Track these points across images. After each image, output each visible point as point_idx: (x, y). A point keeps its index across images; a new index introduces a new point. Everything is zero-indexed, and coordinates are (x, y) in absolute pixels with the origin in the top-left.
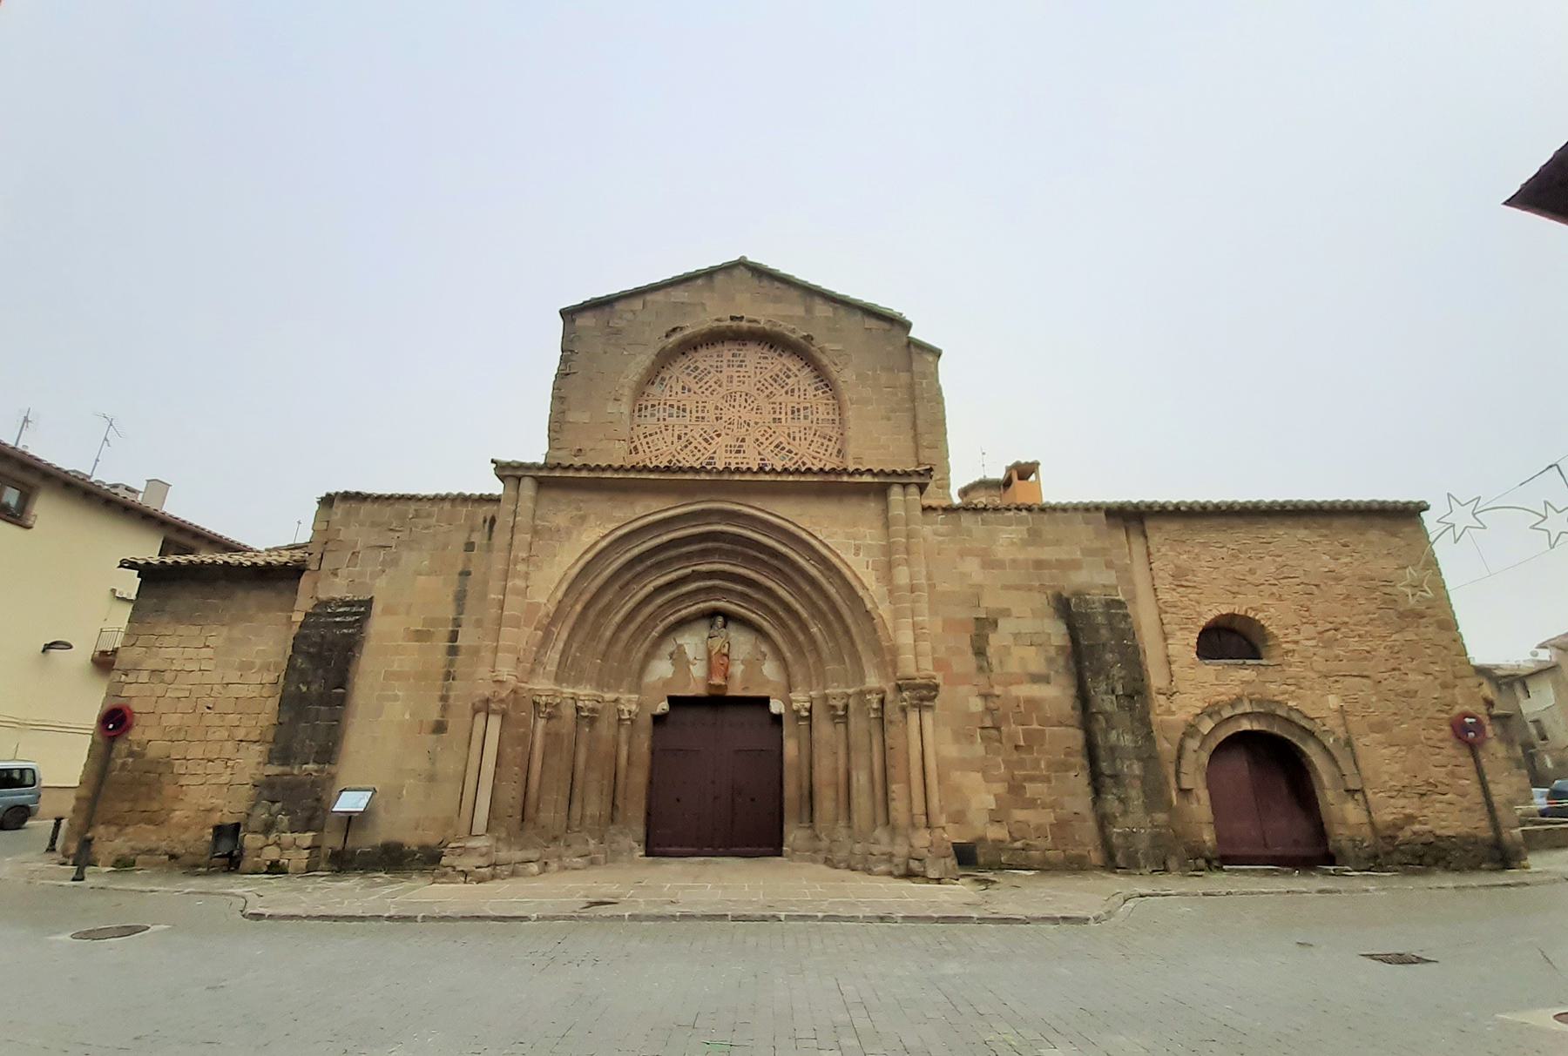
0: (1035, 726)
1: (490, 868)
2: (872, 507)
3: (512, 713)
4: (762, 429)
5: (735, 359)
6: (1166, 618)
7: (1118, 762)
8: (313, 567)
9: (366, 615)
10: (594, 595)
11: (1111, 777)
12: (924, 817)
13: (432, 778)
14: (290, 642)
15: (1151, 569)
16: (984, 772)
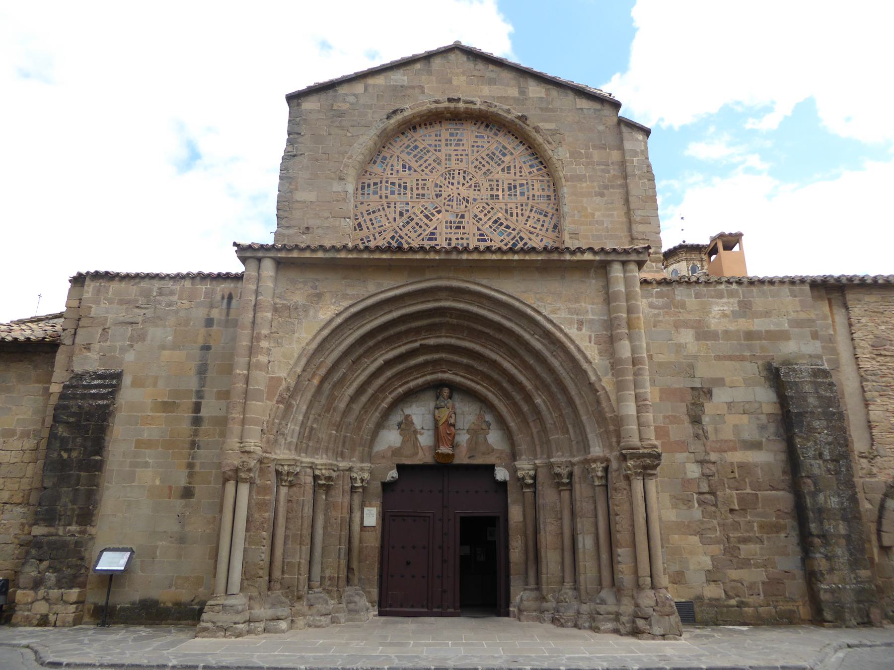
0: (748, 491)
1: (245, 624)
2: (592, 285)
3: (258, 481)
4: (481, 205)
5: (452, 138)
6: (868, 385)
7: (826, 522)
8: (67, 341)
9: (115, 389)
10: (330, 370)
11: (818, 536)
12: (649, 579)
13: (182, 540)
14: (50, 412)
15: (852, 339)
16: (700, 534)
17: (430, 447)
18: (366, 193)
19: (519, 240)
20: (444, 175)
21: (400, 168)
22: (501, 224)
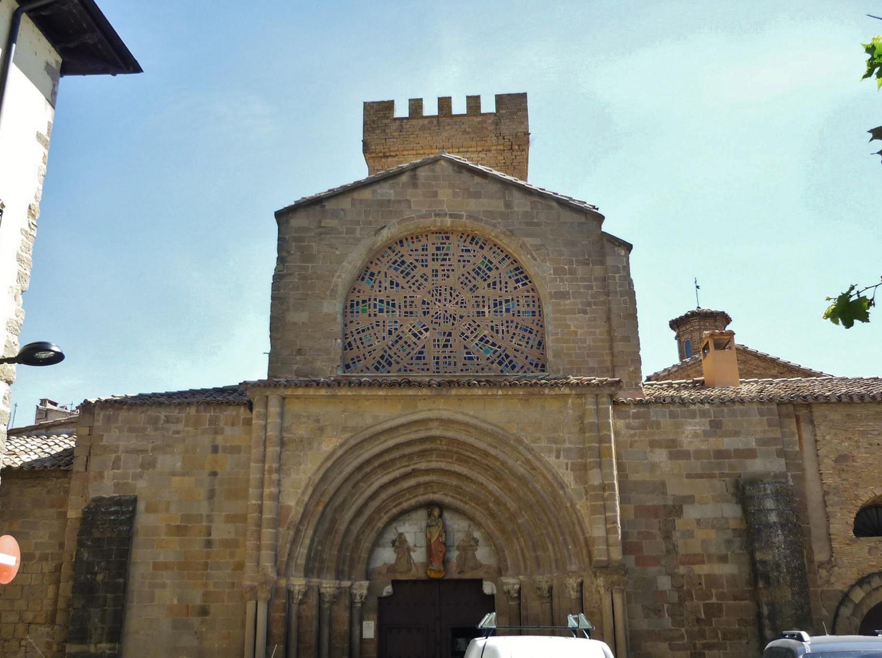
5: (439, 252)
15: (818, 456)
17: (423, 563)
18: (355, 311)
19: (504, 357)
20: (432, 291)
21: (387, 284)
22: (487, 342)
